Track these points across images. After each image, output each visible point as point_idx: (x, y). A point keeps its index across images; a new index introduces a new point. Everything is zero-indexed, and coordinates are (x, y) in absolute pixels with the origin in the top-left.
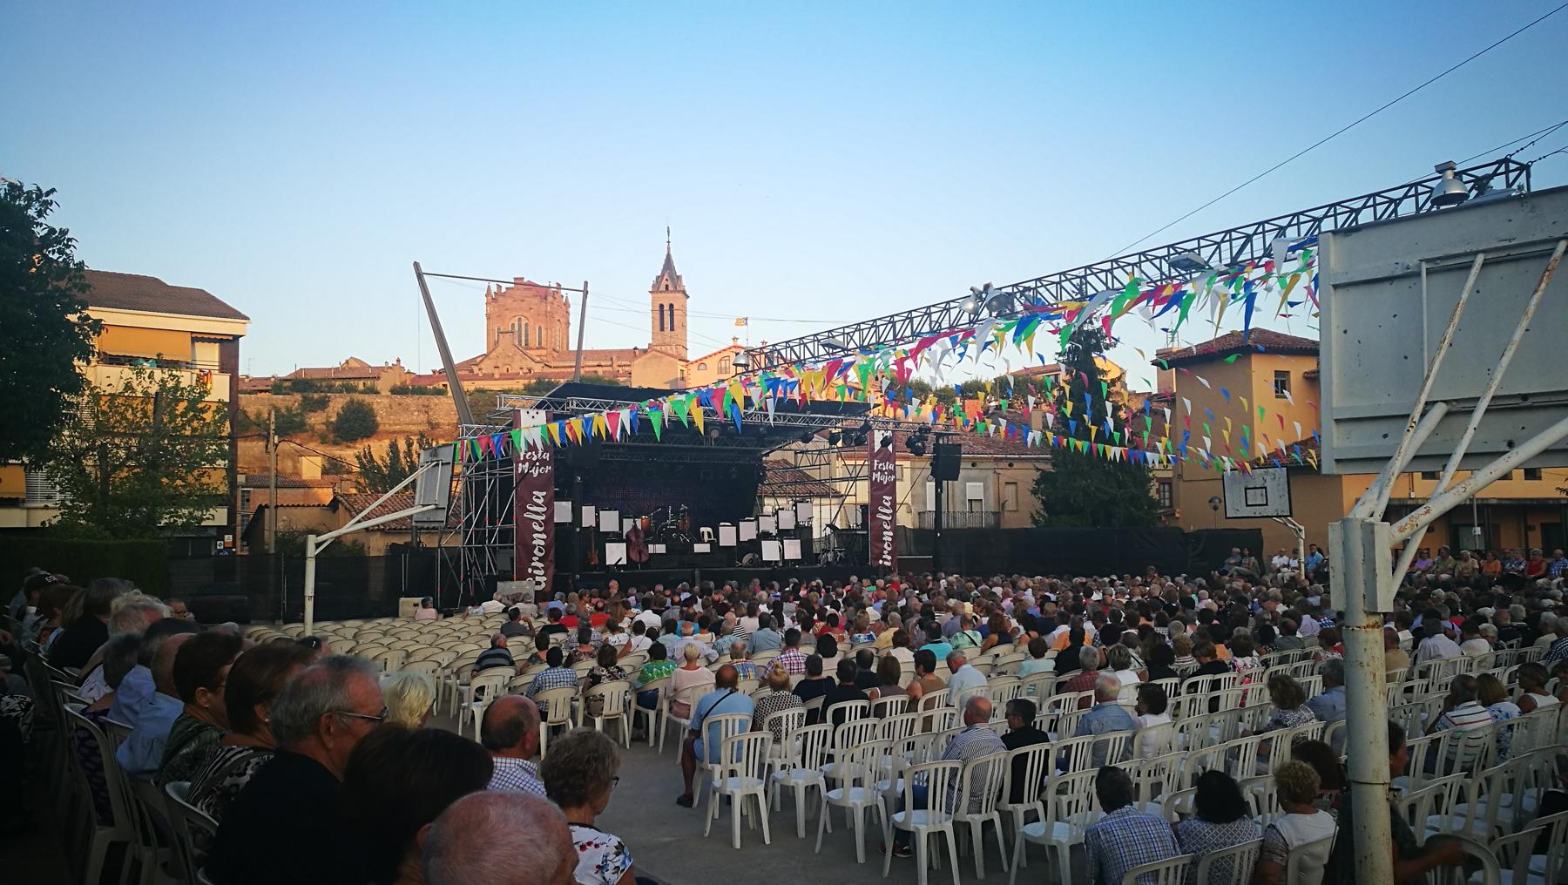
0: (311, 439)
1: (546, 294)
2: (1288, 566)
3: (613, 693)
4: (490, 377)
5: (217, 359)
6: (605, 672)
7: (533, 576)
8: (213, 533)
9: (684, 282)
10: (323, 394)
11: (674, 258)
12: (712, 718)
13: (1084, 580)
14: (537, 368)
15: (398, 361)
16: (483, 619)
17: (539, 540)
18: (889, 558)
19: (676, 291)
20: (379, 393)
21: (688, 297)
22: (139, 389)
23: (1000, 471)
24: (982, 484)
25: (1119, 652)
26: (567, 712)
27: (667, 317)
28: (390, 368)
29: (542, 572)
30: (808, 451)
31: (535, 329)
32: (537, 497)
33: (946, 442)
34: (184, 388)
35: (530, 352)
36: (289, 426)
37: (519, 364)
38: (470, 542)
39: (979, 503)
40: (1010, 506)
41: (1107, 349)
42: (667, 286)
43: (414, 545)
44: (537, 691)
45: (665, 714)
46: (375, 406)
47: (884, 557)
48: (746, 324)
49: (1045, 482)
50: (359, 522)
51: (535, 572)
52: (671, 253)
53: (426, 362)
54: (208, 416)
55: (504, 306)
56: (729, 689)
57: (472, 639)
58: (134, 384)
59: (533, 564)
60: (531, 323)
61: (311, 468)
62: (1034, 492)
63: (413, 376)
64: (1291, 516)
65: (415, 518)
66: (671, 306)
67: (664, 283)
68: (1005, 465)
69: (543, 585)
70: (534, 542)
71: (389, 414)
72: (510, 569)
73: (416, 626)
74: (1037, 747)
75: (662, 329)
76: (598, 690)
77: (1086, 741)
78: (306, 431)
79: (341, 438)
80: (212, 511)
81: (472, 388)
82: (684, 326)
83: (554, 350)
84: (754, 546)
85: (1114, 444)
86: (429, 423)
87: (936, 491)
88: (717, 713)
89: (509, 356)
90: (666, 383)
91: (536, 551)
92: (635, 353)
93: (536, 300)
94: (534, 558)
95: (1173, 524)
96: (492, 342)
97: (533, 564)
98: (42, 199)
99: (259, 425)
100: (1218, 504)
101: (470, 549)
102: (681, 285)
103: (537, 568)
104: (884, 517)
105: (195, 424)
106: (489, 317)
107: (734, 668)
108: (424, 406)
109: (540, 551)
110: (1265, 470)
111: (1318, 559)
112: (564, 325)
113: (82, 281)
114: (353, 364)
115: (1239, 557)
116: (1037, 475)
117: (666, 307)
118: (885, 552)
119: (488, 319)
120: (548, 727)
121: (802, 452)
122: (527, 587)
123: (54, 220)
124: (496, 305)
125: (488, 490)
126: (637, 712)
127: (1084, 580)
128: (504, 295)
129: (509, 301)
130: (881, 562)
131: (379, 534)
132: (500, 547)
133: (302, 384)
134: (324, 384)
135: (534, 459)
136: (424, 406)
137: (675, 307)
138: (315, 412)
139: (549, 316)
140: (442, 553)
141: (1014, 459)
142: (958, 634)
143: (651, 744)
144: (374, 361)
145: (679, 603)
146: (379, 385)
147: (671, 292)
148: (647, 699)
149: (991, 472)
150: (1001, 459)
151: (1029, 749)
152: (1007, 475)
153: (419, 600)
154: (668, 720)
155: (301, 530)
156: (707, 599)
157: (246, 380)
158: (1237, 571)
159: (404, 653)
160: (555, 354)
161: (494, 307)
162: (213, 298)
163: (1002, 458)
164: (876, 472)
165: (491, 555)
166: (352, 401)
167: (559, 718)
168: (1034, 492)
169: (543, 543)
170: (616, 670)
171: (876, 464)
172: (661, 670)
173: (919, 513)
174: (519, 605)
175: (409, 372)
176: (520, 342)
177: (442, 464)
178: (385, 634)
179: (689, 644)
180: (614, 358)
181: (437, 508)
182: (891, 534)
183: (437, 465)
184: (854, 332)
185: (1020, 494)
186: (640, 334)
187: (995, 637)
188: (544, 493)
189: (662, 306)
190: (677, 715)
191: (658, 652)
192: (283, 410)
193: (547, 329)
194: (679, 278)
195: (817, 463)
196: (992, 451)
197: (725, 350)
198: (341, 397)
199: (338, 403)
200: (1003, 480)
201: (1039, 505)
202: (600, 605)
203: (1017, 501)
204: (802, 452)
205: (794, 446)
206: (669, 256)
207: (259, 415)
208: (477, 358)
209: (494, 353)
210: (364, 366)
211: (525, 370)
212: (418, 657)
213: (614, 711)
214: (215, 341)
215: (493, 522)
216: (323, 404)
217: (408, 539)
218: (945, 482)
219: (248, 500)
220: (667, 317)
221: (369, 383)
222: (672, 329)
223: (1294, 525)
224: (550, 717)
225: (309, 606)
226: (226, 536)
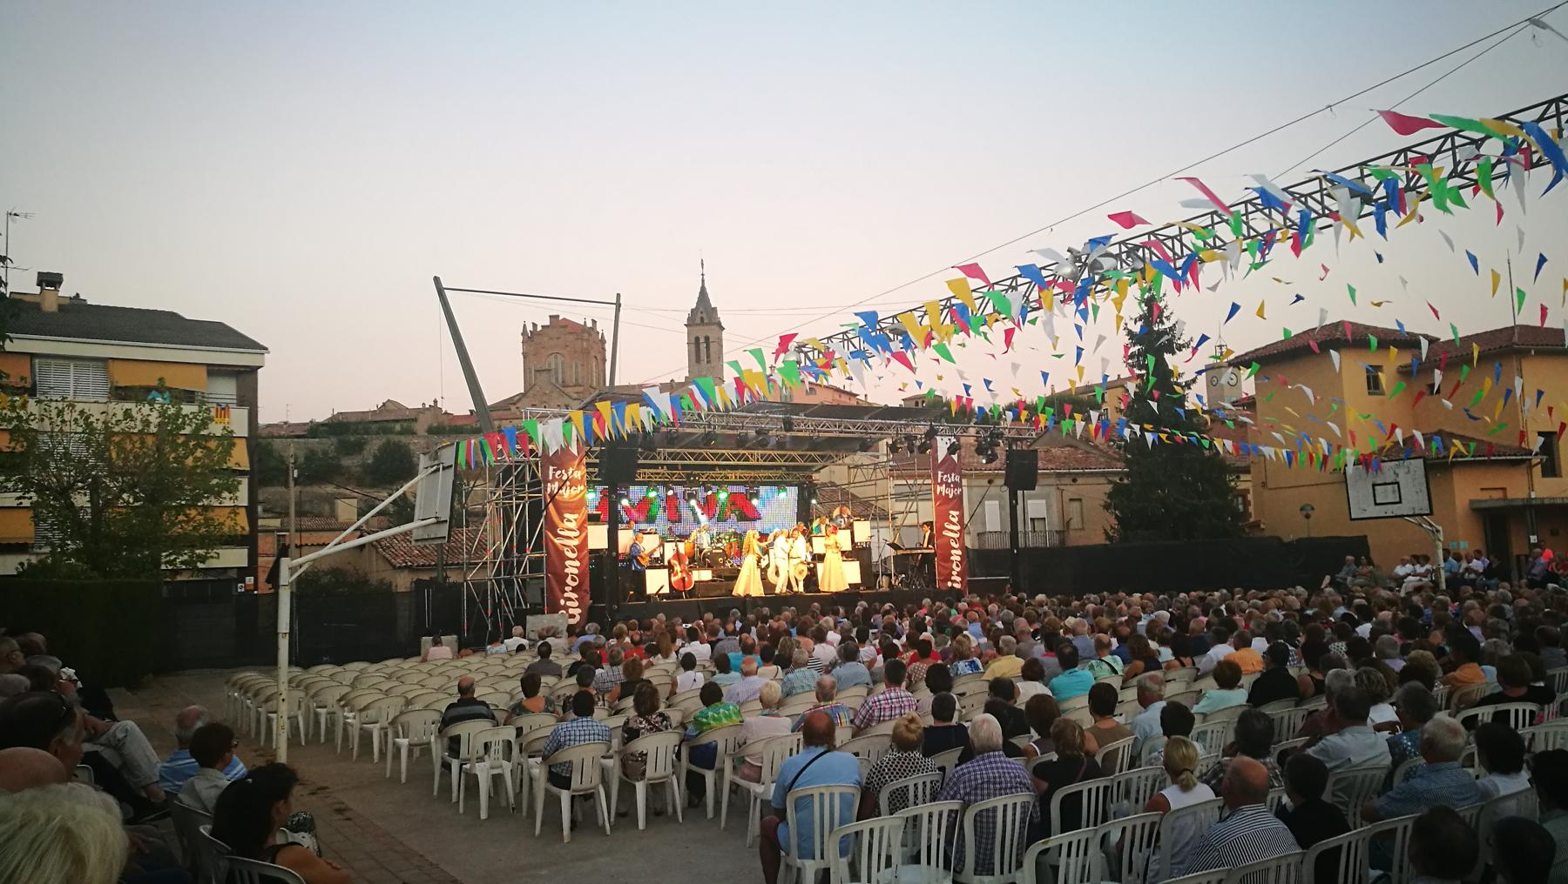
3: (658, 747)
5: (235, 393)
7: (566, 608)
8: (233, 574)
12: (799, 791)
13: (1201, 593)
15: (435, 402)
16: (506, 657)
17: (572, 567)
18: (959, 579)
22: (139, 417)
24: (1044, 502)
25: (1369, 678)
29: (576, 604)
30: (863, 465)
31: (571, 367)
32: (569, 521)
34: (187, 415)
38: (498, 573)
39: (1041, 522)
40: (1075, 523)
41: (1180, 350)
42: (702, 319)
43: (440, 580)
45: (728, 775)
46: (412, 447)
47: (953, 578)
49: (1118, 498)
51: (569, 603)
53: (459, 404)
57: (488, 682)
58: (134, 413)
59: (566, 595)
62: (1107, 507)
64: (1431, 514)
65: (416, 535)
66: (707, 339)
67: (699, 315)
68: (1068, 480)
69: (578, 618)
70: (566, 571)
72: (540, 601)
74: (1093, 784)
75: (698, 360)
78: (343, 474)
81: (510, 426)
87: (1011, 502)
88: (808, 783)
91: (569, 581)
94: (566, 588)
95: (1259, 534)
97: (566, 595)
100: (1310, 512)
101: (498, 582)
102: (716, 317)
103: (570, 599)
105: (199, 453)
106: (525, 355)
109: (573, 579)
111: (1452, 566)
114: (391, 407)
116: (1109, 488)
117: (702, 340)
118: (954, 573)
119: (524, 358)
120: (573, 797)
121: (856, 467)
122: (559, 621)
127: (1201, 593)
129: (546, 339)
131: (406, 572)
132: (531, 579)
133: (343, 429)
135: (565, 478)
139: (586, 352)
141: (1078, 474)
142: (1093, 662)
143: (710, 815)
144: (412, 402)
147: (707, 324)
148: (704, 756)
149: (1053, 489)
151: (1083, 786)
152: (1071, 490)
154: (732, 783)
155: (326, 570)
156: (763, 627)
159: (402, 701)
163: (1065, 473)
164: (941, 484)
165: (520, 588)
166: (388, 442)
168: (1107, 507)
169: (576, 571)
170: (659, 719)
171: (940, 476)
172: (718, 714)
173: (978, 534)
175: (446, 413)
176: (557, 379)
178: (389, 677)
181: (438, 523)
182: (960, 552)
185: (1085, 510)
188: (576, 516)
189: (697, 339)
190: (745, 777)
195: (873, 478)
196: (1050, 466)
199: (375, 444)
200: (1067, 496)
201: (1114, 522)
203: (1082, 519)
204: (856, 467)
205: (847, 460)
209: (531, 392)
213: (660, 773)
215: (522, 550)
216: (358, 447)
218: (1020, 493)
221: (405, 425)
223: (1431, 525)
225: (284, 645)
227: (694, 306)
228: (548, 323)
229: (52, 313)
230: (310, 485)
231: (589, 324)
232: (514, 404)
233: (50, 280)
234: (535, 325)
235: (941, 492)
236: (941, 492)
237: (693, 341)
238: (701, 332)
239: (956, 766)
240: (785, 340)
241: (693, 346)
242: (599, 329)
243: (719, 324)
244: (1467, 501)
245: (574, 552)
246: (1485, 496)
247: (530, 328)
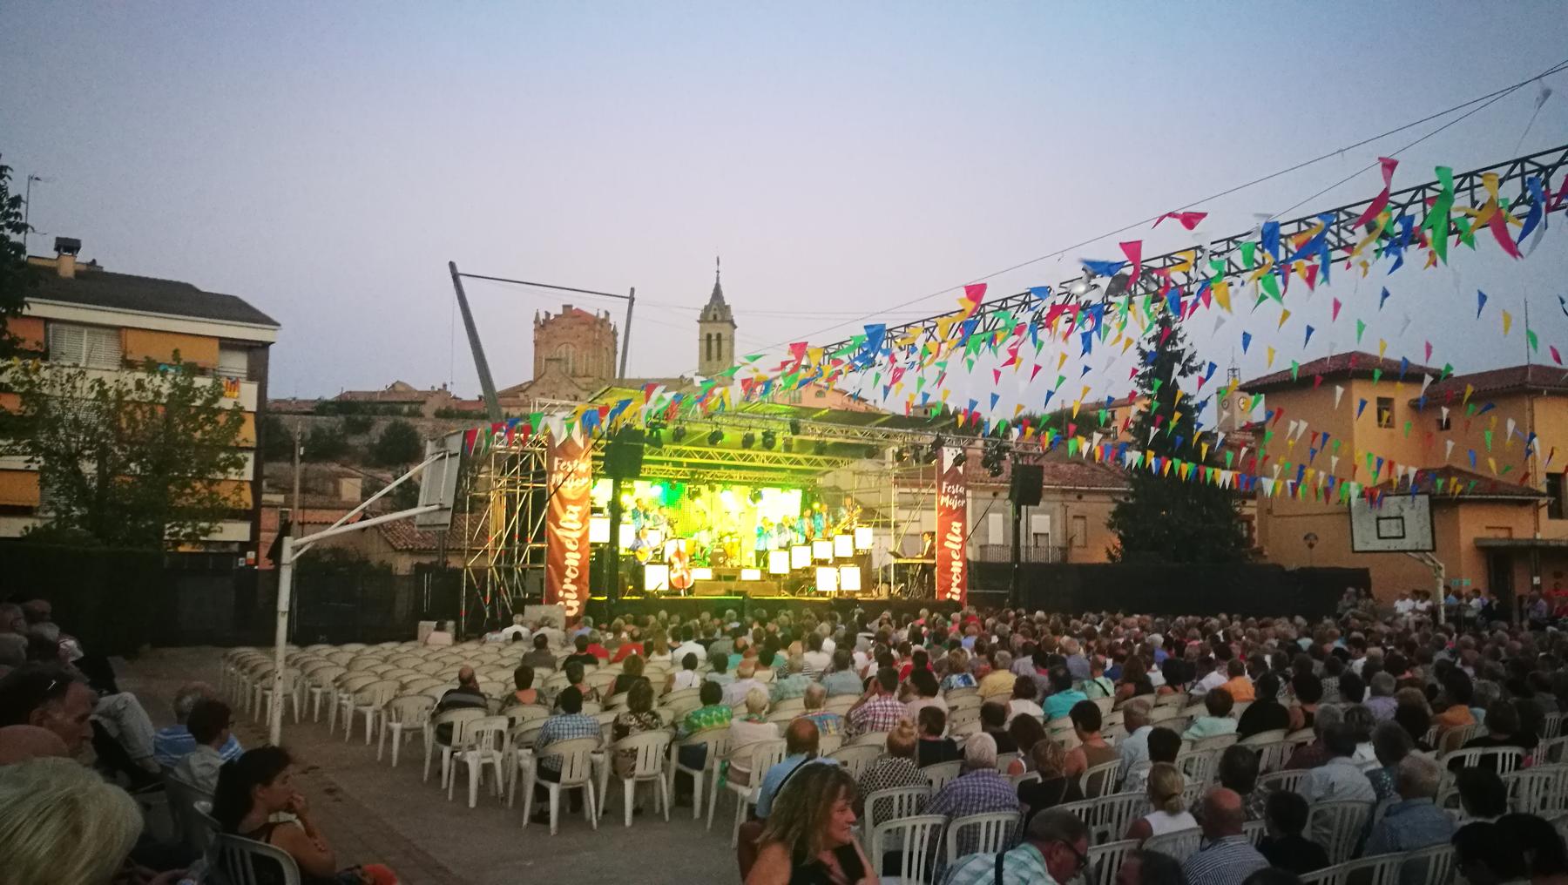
2: (466, 692)
3: (649, 745)
6: (634, 721)
8: (235, 548)
11: (724, 289)
15: (445, 386)
19: (723, 321)
23: (1068, 504)
24: (1048, 517)
26: (586, 772)
28: (436, 393)
33: (1025, 463)
35: (579, 381)
39: (1044, 539)
40: (1078, 541)
42: (715, 317)
44: (546, 744)
45: (716, 777)
46: (418, 429)
50: (347, 523)
51: (567, 595)
52: (721, 282)
53: (468, 389)
54: (222, 419)
56: (807, 753)
65: (419, 520)
68: (1074, 497)
73: (423, 652)
75: (709, 358)
76: (628, 743)
77: (1387, 862)
80: (220, 524)
85: (1224, 468)
89: (554, 383)
91: (568, 572)
95: (1261, 561)
97: (565, 587)
106: (536, 343)
107: (812, 723)
109: (573, 571)
110: (1402, 497)
113: (18, 220)
115: (1355, 599)
116: (1113, 507)
117: (714, 337)
119: (536, 345)
125: (518, 508)
126: (679, 773)
128: (552, 323)
129: (557, 328)
130: (948, 595)
134: (369, 406)
139: (597, 344)
140: (468, 572)
141: (1082, 491)
143: (697, 814)
145: (729, 633)
146: (424, 409)
148: (694, 756)
149: (1058, 505)
150: (1069, 491)
152: (1076, 507)
153: (434, 624)
157: (293, 402)
158: (1352, 614)
159: (397, 685)
163: (1071, 490)
166: (395, 425)
167: (575, 779)
170: (650, 717)
173: (981, 547)
174: (545, 630)
177: (450, 456)
178: (386, 660)
179: (753, 689)
183: (444, 457)
184: (935, 327)
187: (1131, 687)
189: (709, 336)
191: (711, 694)
192: (327, 433)
194: (728, 307)
196: (1056, 482)
198: (384, 419)
199: (382, 425)
200: (1071, 513)
201: (1117, 541)
202: (636, 633)
210: (409, 390)
212: (414, 689)
213: (650, 771)
215: (523, 539)
216: (365, 427)
217: (435, 559)
224: (565, 777)
226: (249, 553)
227: (708, 303)
231: (602, 316)
233: (68, 246)
234: (548, 314)
235: (944, 504)
236: (944, 504)
238: (714, 330)
241: (705, 344)
244: (1472, 541)
245: (574, 543)
246: (1490, 534)
247: (542, 316)
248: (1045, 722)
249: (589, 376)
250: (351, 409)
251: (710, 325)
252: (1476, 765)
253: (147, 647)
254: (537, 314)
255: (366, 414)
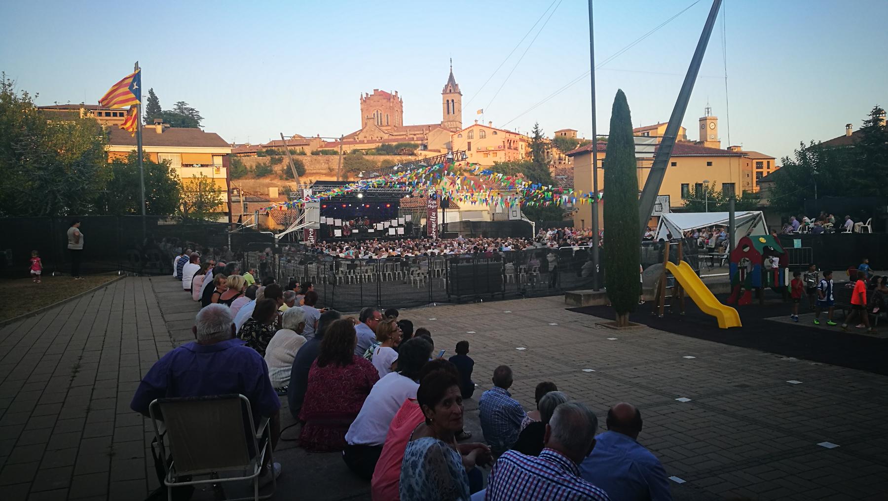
0: (276, 177)
1: (388, 97)
4: (362, 142)
7: (310, 240)
9: (460, 87)
10: (280, 156)
14: (386, 137)
15: (318, 135)
19: (455, 92)
20: (306, 155)
21: (462, 95)
27: (451, 106)
31: (384, 116)
36: (262, 172)
37: (377, 135)
42: (450, 90)
46: (304, 161)
48: (482, 112)
55: (369, 104)
60: (383, 113)
61: (274, 192)
63: (326, 143)
67: (449, 88)
71: (311, 165)
75: (448, 113)
79: (289, 177)
82: (460, 111)
83: (395, 126)
84: (386, 230)
86: (329, 169)
90: (444, 144)
91: (310, 232)
92: (429, 127)
93: (385, 101)
96: (364, 123)
98: (170, 162)
99: (252, 172)
104: (433, 220)
106: (362, 110)
108: (327, 160)
112: (400, 113)
117: (450, 102)
119: (362, 111)
123: (172, 166)
124: (366, 104)
129: (372, 102)
131: (281, 225)
136: (327, 160)
137: (455, 101)
138: (277, 164)
139: (391, 108)
147: (453, 93)
160: (396, 129)
161: (365, 105)
162: (219, 138)
176: (378, 122)
180: (424, 129)
186: (436, 116)
193: (390, 116)
194: (457, 85)
197: (471, 127)
199: (286, 161)
206: (451, 74)
207: (251, 167)
208: (357, 132)
211: (380, 138)
214: (220, 156)
216: (280, 161)
219: (247, 208)
220: (451, 106)
222: (454, 113)
227: (446, 84)
228: (373, 94)
229: (160, 134)
230: (259, 179)
231: (394, 94)
232: (357, 136)
234: (367, 94)
237: (446, 102)
238: (450, 97)
239: (251, 282)
240: (99, 102)
241: (446, 105)
242: (399, 96)
243: (460, 93)
247: (364, 96)
248: (214, 256)
249: (389, 126)
250: (272, 151)
251: (448, 95)
252: (69, 248)
253: (28, 160)
254: (362, 95)
255: (280, 155)
